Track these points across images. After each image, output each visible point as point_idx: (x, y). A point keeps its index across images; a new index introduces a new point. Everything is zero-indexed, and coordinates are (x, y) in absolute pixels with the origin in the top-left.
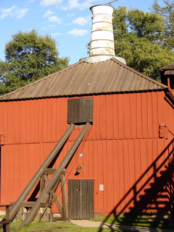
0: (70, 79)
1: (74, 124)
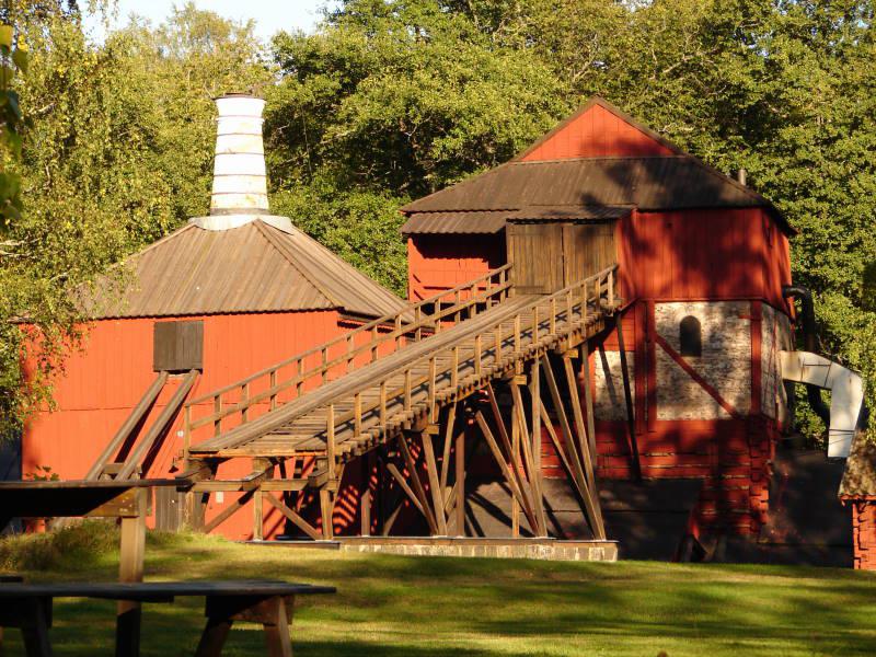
0: (161, 275)
1: (165, 373)
